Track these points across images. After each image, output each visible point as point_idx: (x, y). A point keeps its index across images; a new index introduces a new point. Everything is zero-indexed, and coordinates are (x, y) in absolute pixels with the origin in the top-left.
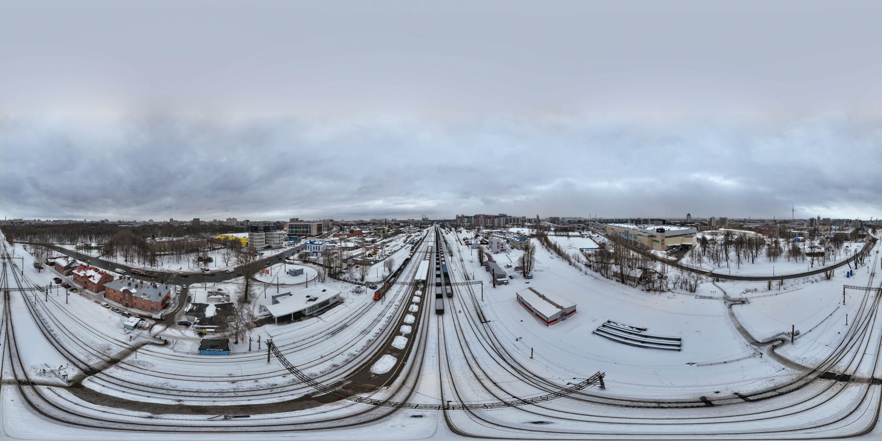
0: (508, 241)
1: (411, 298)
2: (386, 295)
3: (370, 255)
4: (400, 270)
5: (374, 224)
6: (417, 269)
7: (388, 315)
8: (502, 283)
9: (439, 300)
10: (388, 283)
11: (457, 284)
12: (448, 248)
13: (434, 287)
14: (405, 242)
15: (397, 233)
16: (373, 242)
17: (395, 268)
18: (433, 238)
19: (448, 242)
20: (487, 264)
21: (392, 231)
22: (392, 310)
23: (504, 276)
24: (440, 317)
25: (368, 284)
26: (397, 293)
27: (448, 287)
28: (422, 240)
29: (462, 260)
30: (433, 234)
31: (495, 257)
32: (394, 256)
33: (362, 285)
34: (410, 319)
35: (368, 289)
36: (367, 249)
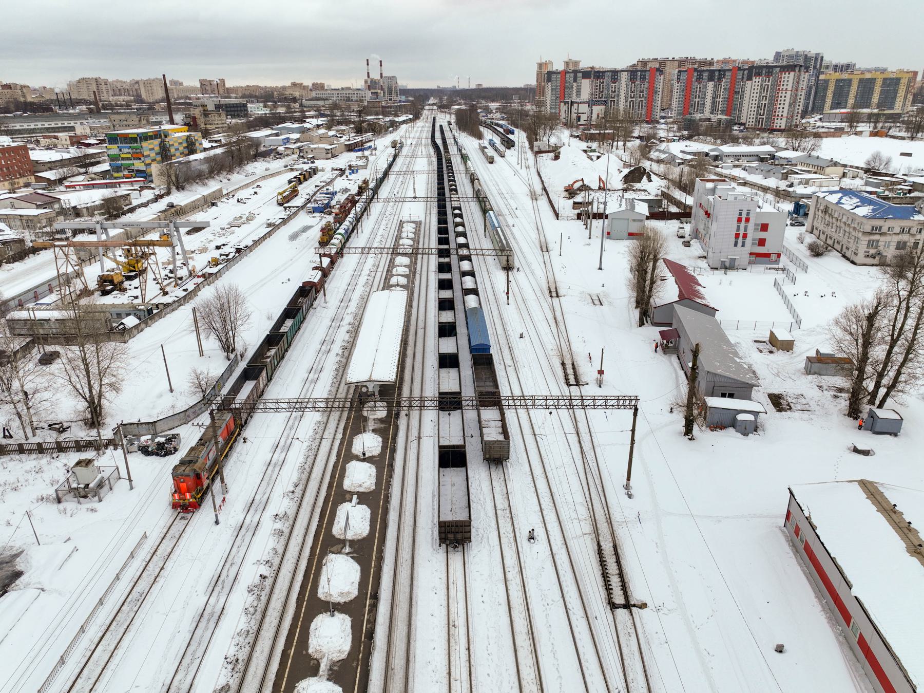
0: (800, 211)
1: (339, 473)
2: (231, 469)
3: (108, 284)
4: (277, 340)
5: (96, 108)
6: (355, 331)
7: (250, 574)
8: (725, 422)
9: (453, 475)
10: (229, 413)
11: (528, 402)
12: (493, 231)
13: (430, 415)
14: (284, 201)
15: (239, 156)
16: (113, 209)
17: (250, 337)
18: (423, 182)
19: (495, 200)
20: (667, 317)
21: (208, 149)
22: (264, 544)
23: (742, 390)
24: (456, 559)
25: (127, 436)
26: (275, 455)
27: (490, 414)
28: (369, 192)
29: (554, 292)
30: (423, 164)
31: (714, 287)
32: (236, 278)
33: (98, 446)
34: (341, 577)
35: (138, 461)
36: (87, 254)
